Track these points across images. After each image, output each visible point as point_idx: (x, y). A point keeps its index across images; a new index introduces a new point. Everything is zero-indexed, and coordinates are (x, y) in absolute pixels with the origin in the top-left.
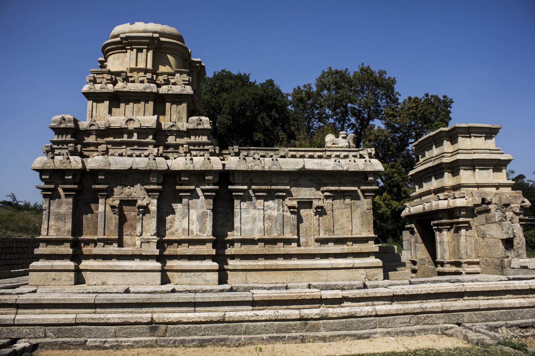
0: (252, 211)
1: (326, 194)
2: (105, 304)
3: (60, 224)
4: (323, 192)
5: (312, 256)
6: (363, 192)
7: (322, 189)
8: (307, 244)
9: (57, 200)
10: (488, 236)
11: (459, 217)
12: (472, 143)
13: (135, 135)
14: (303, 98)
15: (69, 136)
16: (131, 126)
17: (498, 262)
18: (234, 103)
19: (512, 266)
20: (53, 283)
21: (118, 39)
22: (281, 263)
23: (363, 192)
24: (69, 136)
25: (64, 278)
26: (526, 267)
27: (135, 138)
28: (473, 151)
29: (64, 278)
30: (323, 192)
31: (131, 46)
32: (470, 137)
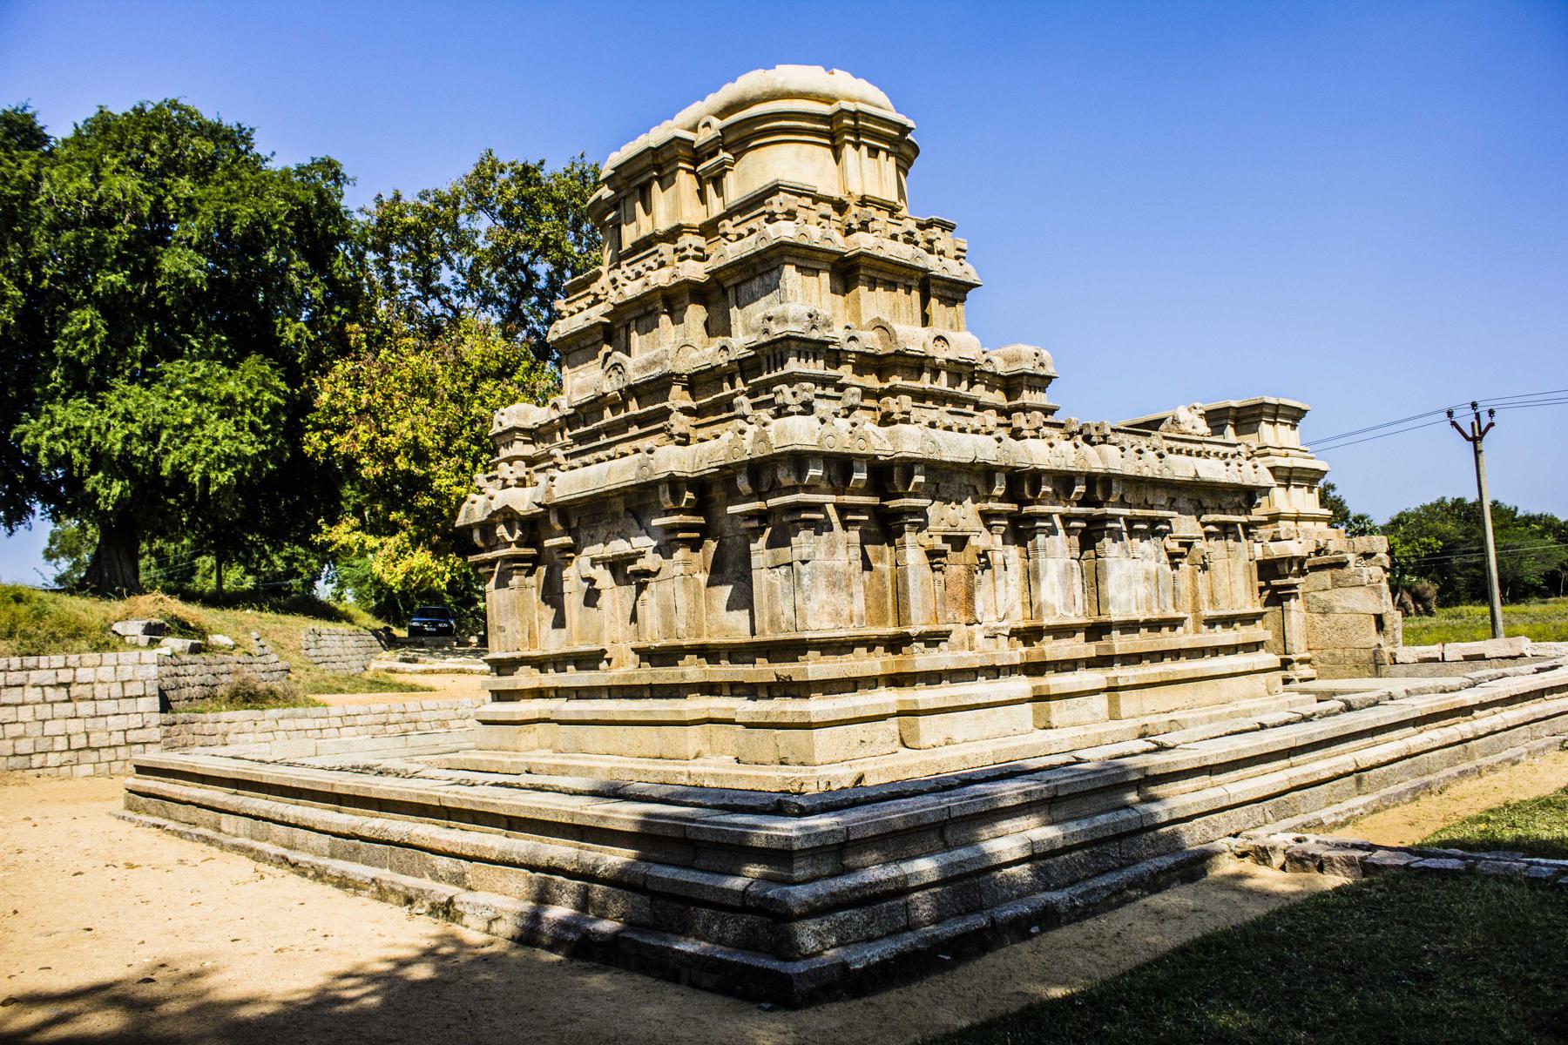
0: (1128, 563)
1: (1211, 528)
2: (525, 819)
3: (841, 598)
4: (1204, 525)
5: (1200, 652)
6: (842, 509)
7: (1204, 518)
8: (763, 632)
9: (825, 534)
10: (1338, 610)
11: (1286, 576)
12: (1277, 435)
13: (943, 375)
14: (421, 234)
15: (821, 363)
16: (941, 354)
17: (1366, 655)
18: (231, 217)
19: (1399, 660)
20: (861, 753)
21: (826, 109)
22: (1168, 668)
23: (842, 509)
24: (821, 363)
25: (880, 739)
26: (1482, 657)
27: (942, 384)
28: (1283, 452)
29: (880, 739)
30: (1204, 525)
31: (858, 136)
32: (1274, 424)
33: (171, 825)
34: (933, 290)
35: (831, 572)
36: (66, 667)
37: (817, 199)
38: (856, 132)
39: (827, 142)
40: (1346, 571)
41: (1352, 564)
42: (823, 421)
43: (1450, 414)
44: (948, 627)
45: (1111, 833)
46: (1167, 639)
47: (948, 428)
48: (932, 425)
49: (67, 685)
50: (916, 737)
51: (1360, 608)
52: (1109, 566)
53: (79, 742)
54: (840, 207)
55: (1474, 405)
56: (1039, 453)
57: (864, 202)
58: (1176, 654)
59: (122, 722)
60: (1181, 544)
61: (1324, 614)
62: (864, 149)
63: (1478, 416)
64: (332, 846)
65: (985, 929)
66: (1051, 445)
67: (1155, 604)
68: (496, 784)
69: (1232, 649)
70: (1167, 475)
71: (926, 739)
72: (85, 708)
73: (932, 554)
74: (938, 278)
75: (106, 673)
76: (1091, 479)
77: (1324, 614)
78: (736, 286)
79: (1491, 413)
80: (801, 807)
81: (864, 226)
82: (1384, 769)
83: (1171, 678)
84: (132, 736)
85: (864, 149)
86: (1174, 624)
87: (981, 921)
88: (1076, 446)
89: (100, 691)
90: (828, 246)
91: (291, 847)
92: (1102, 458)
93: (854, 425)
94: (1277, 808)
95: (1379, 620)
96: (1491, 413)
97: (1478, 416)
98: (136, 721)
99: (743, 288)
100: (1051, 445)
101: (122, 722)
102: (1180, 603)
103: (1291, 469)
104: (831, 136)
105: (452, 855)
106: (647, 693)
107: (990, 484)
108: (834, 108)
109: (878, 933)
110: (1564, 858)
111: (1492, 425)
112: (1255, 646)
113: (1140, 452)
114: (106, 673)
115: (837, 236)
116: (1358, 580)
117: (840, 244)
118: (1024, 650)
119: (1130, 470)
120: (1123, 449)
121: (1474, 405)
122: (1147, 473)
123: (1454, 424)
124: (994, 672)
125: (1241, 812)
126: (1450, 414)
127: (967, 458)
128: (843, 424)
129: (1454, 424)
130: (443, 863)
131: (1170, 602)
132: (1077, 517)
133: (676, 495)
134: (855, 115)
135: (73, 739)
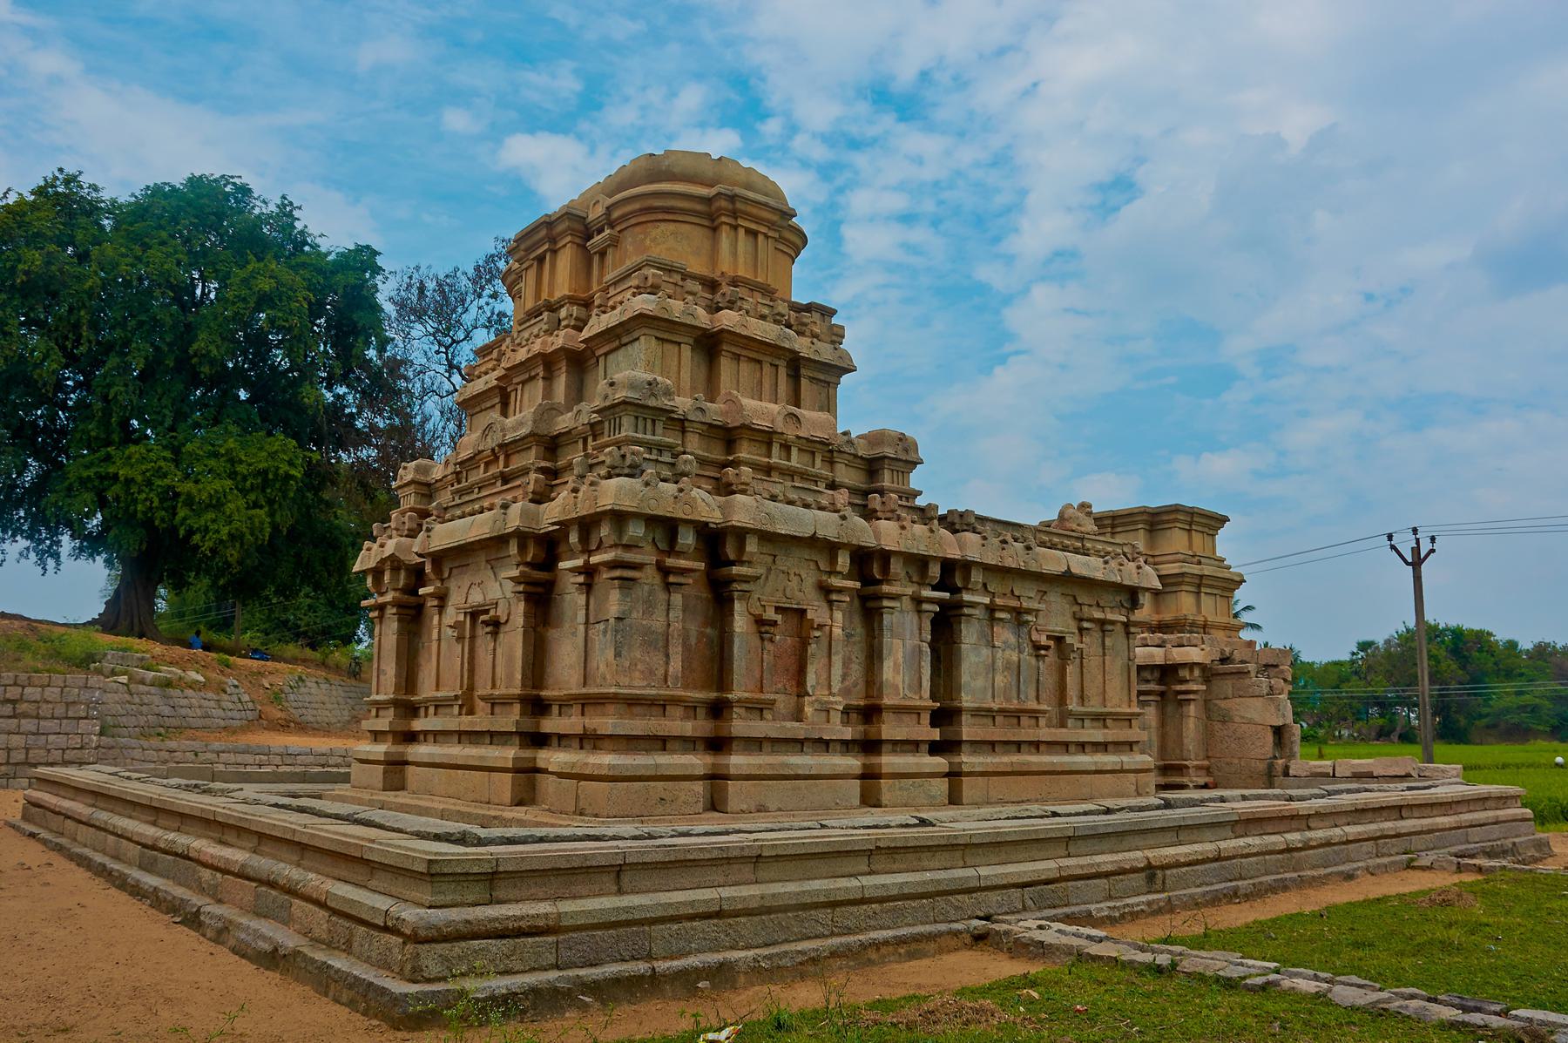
13: (794, 451)
17: (1262, 766)
19: (1291, 772)
20: (660, 810)
26: (1370, 776)
27: (796, 460)
33: (44, 834)
34: (803, 371)
35: (647, 632)
36: (15, 684)
37: (686, 276)
38: (735, 214)
39: (706, 223)
40: (1247, 681)
41: (1253, 674)
42: (647, 484)
43: (1390, 537)
44: (772, 696)
45: (822, 899)
46: (1026, 733)
47: (791, 503)
48: (773, 498)
49: (14, 702)
50: (725, 800)
51: (1257, 718)
52: (964, 653)
53: (18, 756)
54: (712, 285)
55: (1415, 531)
56: (887, 534)
57: (735, 282)
58: (1036, 745)
59: (61, 741)
60: (1049, 637)
61: (1224, 722)
62: (741, 232)
63: (1418, 541)
64: (142, 856)
65: (642, 976)
66: (903, 528)
67: (1014, 694)
68: (276, 805)
69: (1103, 747)
70: (1034, 567)
71: (734, 803)
72: (28, 725)
73: (760, 622)
74: (809, 359)
75: (52, 693)
76: (948, 566)
77: (1224, 722)
78: (606, 354)
79: (1433, 539)
80: (479, 838)
81: (731, 305)
82: (1184, 869)
83: (1025, 769)
84: (69, 755)
85: (741, 232)
86: (1034, 715)
87: (642, 967)
88: (932, 531)
89: (45, 710)
90: (689, 320)
91: (116, 858)
92: (877, 535)
93: (681, 490)
94: (1041, 896)
95: (1278, 731)
96: (1433, 539)
97: (1418, 541)
98: (76, 741)
99: (611, 357)
100: (903, 528)
101: (61, 741)
102: (1043, 695)
103: (1201, 577)
104: (711, 217)
105: (217, 869)
106: (488, 740)
107: (833, 560)
108: (713, 191)
109: (518, 967)
110: (1559, 1008)
111: (1432, 551)
112: (1130, 745)
113: (1004, 542)
114: (52, 693)
115: (701, 311)
116: (1257, 691)
117: (702, 318)
118: (861, 728)
119: (991, 559)
120: (985, 538)
121: (1415, 531)
122: (1010, 563)
123: (1393, 547)
124: (824, 745)
125: (994, 897)
126: (1390, 537)
127: (807, 532)
128: (669, 488)
129: (1393, 547)
130: (206, 874)
131: (1032, 694)
132: (931, 601)
133: (522, 548)
134: (733, 198)
135: (13, 754)
